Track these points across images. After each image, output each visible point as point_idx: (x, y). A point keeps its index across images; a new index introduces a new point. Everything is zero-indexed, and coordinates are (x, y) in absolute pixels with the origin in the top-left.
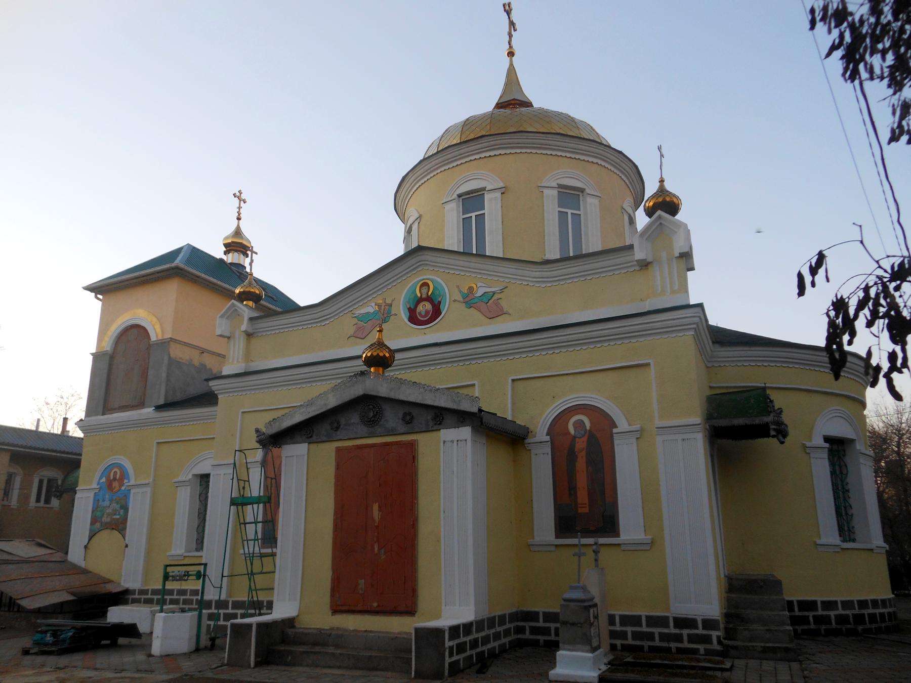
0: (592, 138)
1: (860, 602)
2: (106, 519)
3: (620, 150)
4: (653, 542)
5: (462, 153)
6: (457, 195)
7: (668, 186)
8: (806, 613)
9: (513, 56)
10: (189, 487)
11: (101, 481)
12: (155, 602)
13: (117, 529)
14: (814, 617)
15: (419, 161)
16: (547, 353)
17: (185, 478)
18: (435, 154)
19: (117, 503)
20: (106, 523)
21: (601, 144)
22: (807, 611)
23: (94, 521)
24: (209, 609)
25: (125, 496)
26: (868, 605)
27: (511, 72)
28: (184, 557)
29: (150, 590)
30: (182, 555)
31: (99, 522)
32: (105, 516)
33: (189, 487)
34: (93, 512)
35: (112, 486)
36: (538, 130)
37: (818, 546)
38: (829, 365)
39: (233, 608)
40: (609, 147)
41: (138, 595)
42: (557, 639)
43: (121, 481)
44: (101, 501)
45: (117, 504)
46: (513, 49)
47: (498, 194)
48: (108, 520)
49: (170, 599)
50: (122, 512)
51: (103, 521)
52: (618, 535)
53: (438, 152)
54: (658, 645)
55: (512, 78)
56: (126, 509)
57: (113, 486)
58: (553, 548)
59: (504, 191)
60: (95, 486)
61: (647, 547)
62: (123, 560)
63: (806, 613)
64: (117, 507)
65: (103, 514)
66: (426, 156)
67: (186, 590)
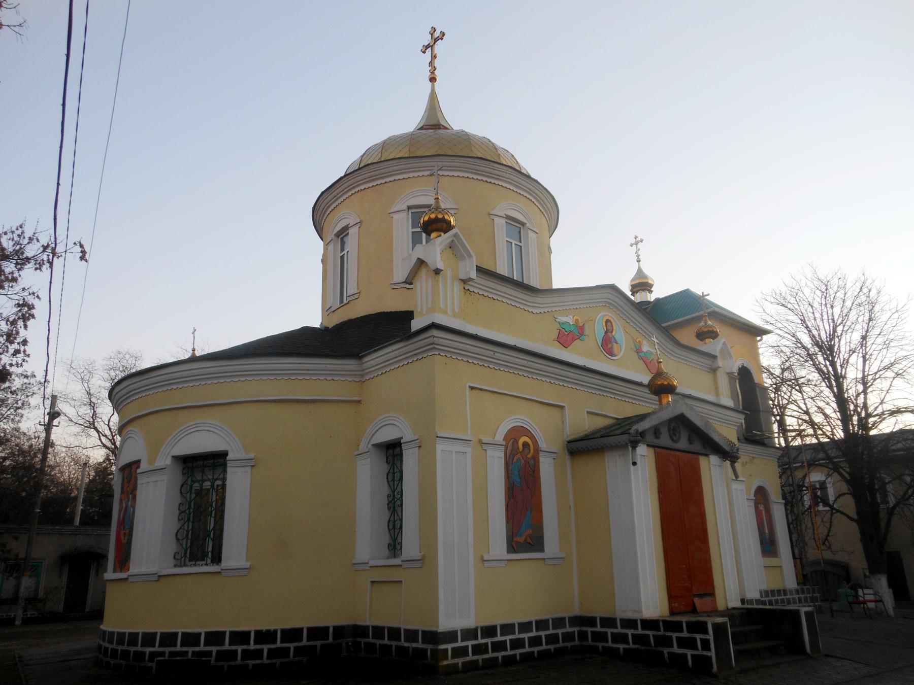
0: (510, 165)
3: (536, 179)
4: (422, 560)
5: (386, 172)
6: (408, 206)
9: (435, 82)
14: (592, 632)
15: (340, 177)
16: (200, 384)
18: (356, 170)
21: (520, 172)
22: (672, 631)
27: (433, 97)
28: (160, 576)
30: (156, 574)
36: (456, 153)
37: (485, 562)
38: (658, 403)
39: (493, 651)
40: (528, 177)
46: (435, 75)
53: (359, 169)
54: (280, 646)
61: (418, 564)
66: (348, 172)
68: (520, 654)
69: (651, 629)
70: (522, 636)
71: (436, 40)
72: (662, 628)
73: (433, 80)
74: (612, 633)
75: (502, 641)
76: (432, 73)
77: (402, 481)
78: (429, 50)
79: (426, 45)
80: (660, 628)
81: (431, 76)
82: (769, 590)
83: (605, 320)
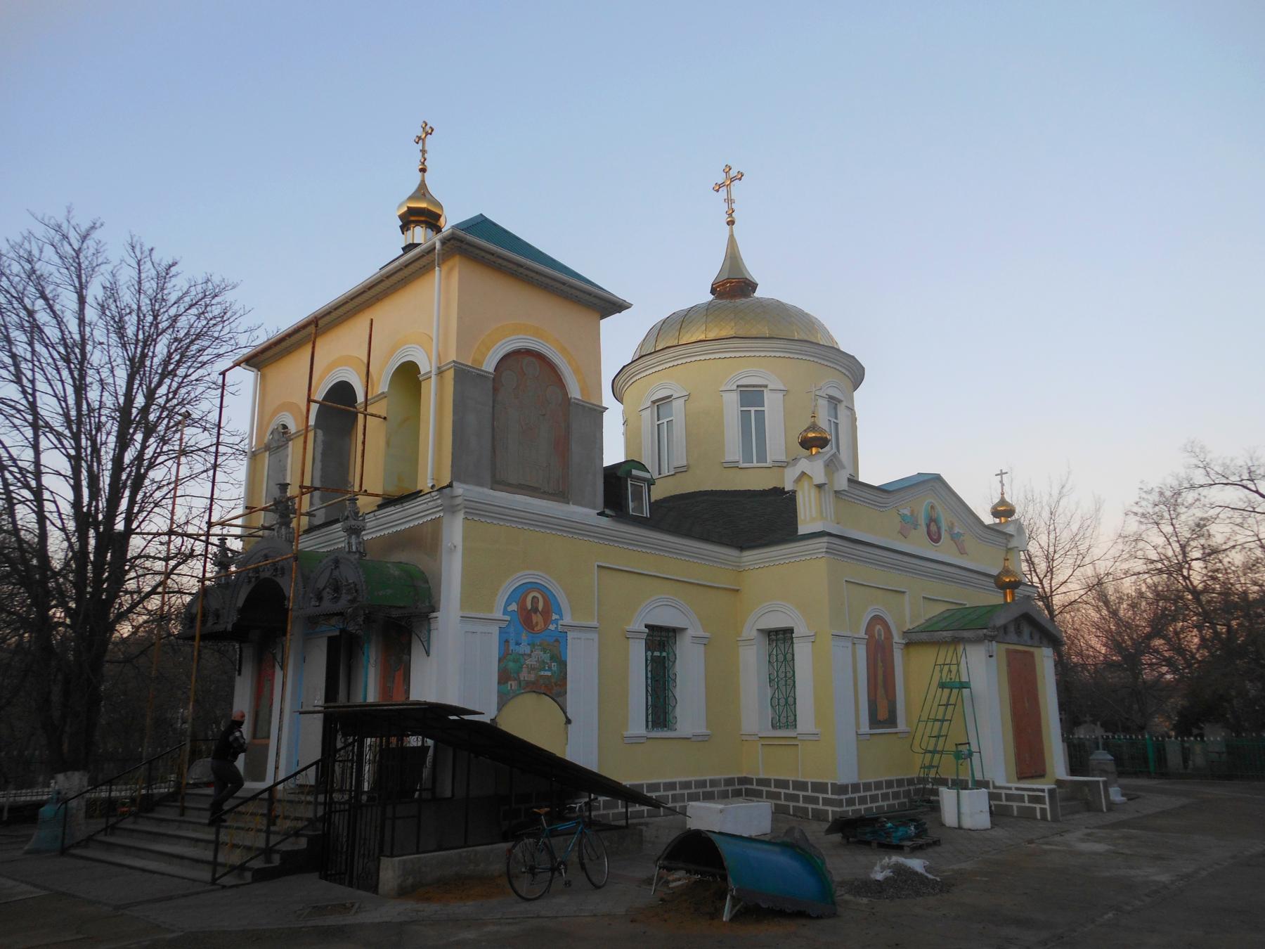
1: (898, 781)
2: (525, 675)
7: (1008, 499)
8: (816, 795)
10: (755, 647)
11: (510, 609)
12: (744, 793)
13: (548, 693)
17: (638, 627)
19: (544, 650)
20: (528, 683)
23: (504, 677)
24: (846, 794)
25: (557, 641)
26: (812, 787)
27: (732, 240)
29: (693, 782)
31: (515, 680)
32: (525, 670)
33: (755, 647)
34: (500, 660)
35: (532, 622)
41: (711, 787)
42: (1046, 791)
43: (546, 614)
44: (512, 642)
45: (545, 653)
47: (780, 395)
48: (532, 677)
49: (688, 793)
50: (554, 666)
51: (522, 679)
52: (896, 726)
55: (733, 258)
56: (563, 665)
57: (534, 622)
58: (868, 737)
59: (786, 392)
60: (498, 614)
62: (566, 744)
63: (816, 795)
64: (546, 657)
65: (521, 667)
67: (659, 784)
68: (852, 810)
69: (755, 790)
70: (888, 791)
71: (732, 180)
72: (755, 783)
73: (731, 223)
74: (812, 809)
75: (852, 798)
76: (730, 215)
77: (795, 687)
78: (723, 191)
79: (720, 183)
80: (789, 787)
81: (729, 219)
82: (940, 799)
83: (940, 543)
